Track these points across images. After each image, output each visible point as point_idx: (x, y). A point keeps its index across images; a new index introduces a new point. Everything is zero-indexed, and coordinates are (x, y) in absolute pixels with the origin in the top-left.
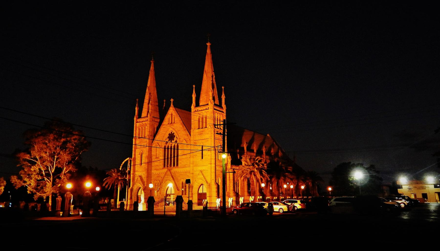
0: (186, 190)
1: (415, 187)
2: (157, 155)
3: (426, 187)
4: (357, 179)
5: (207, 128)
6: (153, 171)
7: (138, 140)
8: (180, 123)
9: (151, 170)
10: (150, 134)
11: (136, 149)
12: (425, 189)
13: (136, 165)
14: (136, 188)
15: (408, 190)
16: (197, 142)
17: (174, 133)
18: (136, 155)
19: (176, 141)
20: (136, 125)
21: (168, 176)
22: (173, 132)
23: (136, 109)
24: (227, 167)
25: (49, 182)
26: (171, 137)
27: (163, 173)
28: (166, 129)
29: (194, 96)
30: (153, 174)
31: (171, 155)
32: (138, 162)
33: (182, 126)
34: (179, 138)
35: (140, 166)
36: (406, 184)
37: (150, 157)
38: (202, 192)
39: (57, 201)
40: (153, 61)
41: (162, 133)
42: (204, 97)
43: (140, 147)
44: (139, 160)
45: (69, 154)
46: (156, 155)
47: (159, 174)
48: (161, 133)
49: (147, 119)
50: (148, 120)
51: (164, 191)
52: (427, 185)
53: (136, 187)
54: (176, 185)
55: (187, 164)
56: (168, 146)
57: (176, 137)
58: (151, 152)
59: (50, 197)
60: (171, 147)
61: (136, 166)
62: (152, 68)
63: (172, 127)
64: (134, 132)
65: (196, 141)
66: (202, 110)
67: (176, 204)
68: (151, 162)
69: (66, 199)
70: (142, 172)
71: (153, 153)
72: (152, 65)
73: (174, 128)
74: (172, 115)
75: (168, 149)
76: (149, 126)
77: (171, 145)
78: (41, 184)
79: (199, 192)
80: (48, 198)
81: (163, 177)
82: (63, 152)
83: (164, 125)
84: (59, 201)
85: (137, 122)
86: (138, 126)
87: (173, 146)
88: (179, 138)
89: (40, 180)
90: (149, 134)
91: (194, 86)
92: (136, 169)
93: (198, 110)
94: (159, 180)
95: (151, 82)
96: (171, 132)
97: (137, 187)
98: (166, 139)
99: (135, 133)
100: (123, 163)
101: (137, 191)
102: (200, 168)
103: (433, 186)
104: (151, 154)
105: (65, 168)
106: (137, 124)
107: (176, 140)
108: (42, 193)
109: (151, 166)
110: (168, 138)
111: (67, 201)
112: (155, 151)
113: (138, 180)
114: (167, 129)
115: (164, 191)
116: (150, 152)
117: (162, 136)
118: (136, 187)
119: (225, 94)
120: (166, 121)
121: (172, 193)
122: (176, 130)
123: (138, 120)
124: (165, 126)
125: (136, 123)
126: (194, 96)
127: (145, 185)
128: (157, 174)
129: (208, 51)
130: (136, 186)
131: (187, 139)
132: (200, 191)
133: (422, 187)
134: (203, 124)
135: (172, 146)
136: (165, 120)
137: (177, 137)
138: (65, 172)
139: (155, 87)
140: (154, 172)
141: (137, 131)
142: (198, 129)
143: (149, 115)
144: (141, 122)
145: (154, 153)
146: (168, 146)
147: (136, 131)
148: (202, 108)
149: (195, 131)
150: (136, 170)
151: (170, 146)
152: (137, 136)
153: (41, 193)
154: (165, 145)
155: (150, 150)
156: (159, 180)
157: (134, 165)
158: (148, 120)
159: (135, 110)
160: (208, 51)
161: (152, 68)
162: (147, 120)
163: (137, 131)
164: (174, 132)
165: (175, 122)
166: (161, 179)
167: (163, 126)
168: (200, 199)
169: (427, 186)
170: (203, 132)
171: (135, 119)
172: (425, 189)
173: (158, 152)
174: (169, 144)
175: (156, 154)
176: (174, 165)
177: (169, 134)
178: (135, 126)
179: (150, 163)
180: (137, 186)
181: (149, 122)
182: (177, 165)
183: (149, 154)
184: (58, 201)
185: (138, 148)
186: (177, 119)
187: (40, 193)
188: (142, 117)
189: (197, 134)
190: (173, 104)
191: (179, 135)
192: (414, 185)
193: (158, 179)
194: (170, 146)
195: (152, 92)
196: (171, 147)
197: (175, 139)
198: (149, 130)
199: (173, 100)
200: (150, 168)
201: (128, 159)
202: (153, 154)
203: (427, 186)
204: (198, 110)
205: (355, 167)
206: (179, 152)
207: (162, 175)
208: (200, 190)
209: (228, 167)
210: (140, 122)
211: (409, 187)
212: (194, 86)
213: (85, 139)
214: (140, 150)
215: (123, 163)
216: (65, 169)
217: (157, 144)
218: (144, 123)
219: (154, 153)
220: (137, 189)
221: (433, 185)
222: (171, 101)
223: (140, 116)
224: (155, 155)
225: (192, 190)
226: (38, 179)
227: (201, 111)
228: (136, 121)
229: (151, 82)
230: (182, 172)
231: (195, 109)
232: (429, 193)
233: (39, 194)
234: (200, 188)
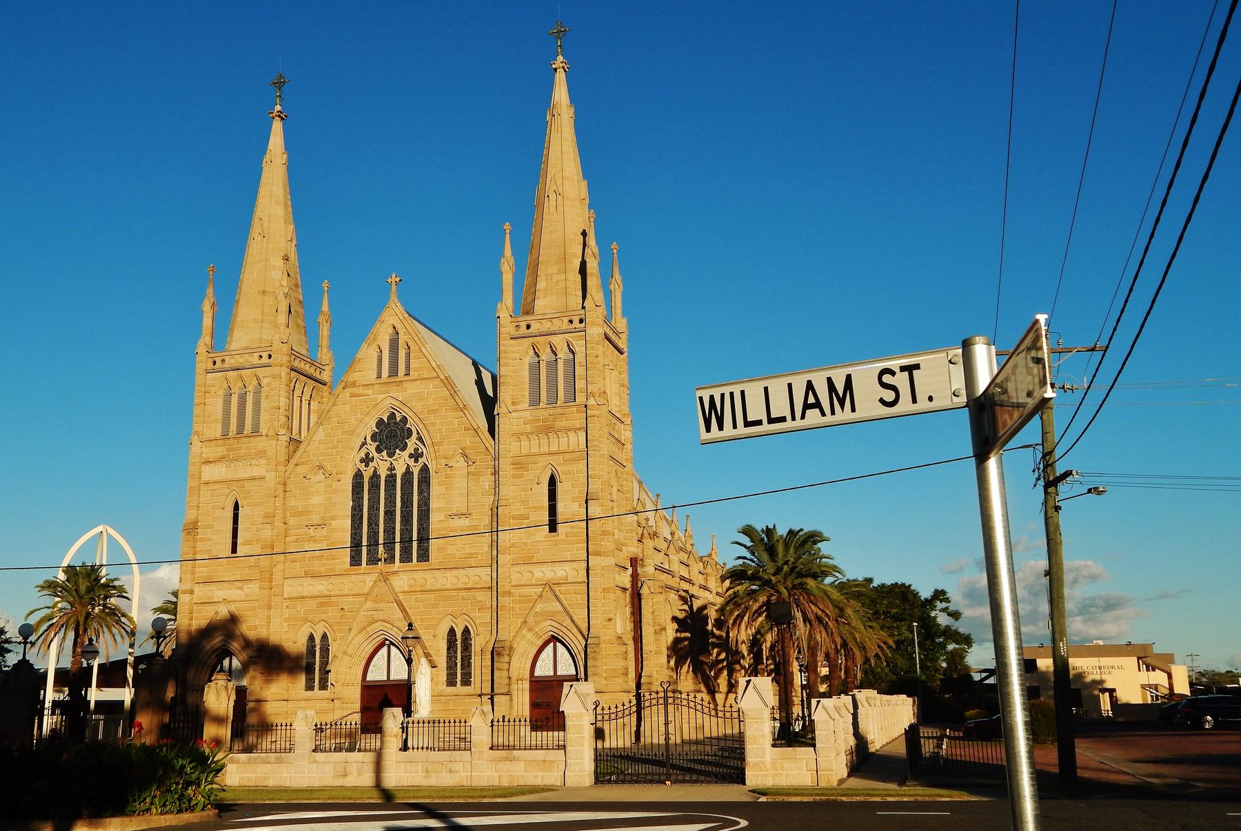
0: (469, 665)
17: (404, 420)
24: (639, 570)
38: (386, 679)
42: (555, 278)
54: (1052, 612)
56: (375, 476)
57: (415, 435)
60: (391, 478)
62: (561, 94)
72: (560, 77)
75: (375, 484)
77: (392, 469)
87: (400, 471)
96: (392, 416)
98: (364, 444)
107: (416, 450)
110: (374, 437)
137: (420, 439)
146: (375, 476)
151: (383, 473)
161: (561, 94)
174: (382, 465)
176: (406, 558)
177: (380, 423)
182: (424, 556)
194: (383, 473)
196: (391, 478)
197: (412, 443)
201: (100, 528)
205: (998, 596)
208: (538, 664)
209: (646, 569)
225: (509, 663)
234: (543, 656)
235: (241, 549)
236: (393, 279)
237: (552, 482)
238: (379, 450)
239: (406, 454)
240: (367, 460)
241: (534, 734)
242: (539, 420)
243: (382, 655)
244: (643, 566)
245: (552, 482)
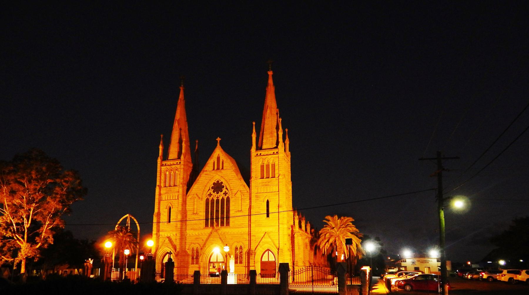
1: (419, 261)
2: (195, 209)
3: (429, 261)
4: (369, 251)
5: (275, 177)
6: (188, 231)
7: (163, 190)
8: (232, 170)
9: (186, 230)
10: (185, 182)
11: (161, 200)
12: (428, 263)
13: (160, 222)
14: (162, 253)
15: (411, 263)
16: (260, 195)
17: (222, 183)
18: (161, 209)
19: (225, 194)
20: (161, 171)
21: (215, 239)
22: (220, 180)
23: (161, 147)
24: (294, 230)
25: (20, 240)
26: (218, 187)
27: (202, 234)
28: (209, 177)
29: (254, 136)
30: (188, 235)
31: (217, 211)
32: (164, 217)
33: (235, 174)
34: (231, 190)
35: (167, 224)
36: (410, 257)
37: (184, 213)
38: (267, 260)
39: (86, 268)
40: (183, 88)
41: (204, 181)
43: (166, 199)
44: (165, 216)
45: (59, 201)
46: (194, 210)
47: (198, 236)
48: (201, 181)
49: (178, 162)
50: (180, 163)
51: (207, 258)
52: (431, 258)
53: (161, 252)
55: (244, 223)
57: (225, 187)
58: (186, 206)
59: (23, 263)
60: (218, 201)
61: (161, 224)
62: (181, 96)
63: (219, 174)
64: (158, 178)
65: (259, 194)
66: (267, 155)
67: (280, 274)
68: (186, 221)
69: (106, 265)
70: (171, 232)
71: (189, 207)
73: (222, 176)
74: (218, 158)
76: (182, 171)
77: (217, 198)
78: (7, 244)
79: (262, 260)
80: (19, 265)
81: (205, 239)
82: (52, 198)
83: (206, 171)
84: (89, 269)
85: (162, 165)
86: (163, 171)
87: (220, 198)
88: (231, 190)
89: (10, 238)
90: (183, 182)
91: (254, 123)
92: (161, 227)
93: (261, 154)
94: (198, 243)
95: (180, 114)
97: (164, 252)
99: (159, 179)
100: (121, 220)
101: (162, 258)
102: (264, 229)
103: (436, 260)
104: (186, 209)
105: (49, 222)
106: (162, 167)
107: (225, 192)
108: (9, 257)
109: (186, 224)
110: (212, 188)
111: (108, 269)
112: (192, 205)
113: (165, 242)
114: (211, 177)
115: (207, 257)
116: (184, 205)
117: (203, 186)
118: (161, 252)
119: (288, 138)
120: (209, 166)
121: (218, 261)
122: (226, 178)
123: (164, 163)
124: (208, 173)
125: (161, 166)
126: (254, 136)
127: (177, 250)
128: (195, 236)
129: (271, 81)
130: (162, 251)
131: (244, 192)
132: (265, 259)
133: (425, 261)
134: (165, 182)
135: (219, 200)
136: (208, 165)
137: (227, 188)
138: (46, 228)
139: (186, 121)
140: (189, 232)
141: (163, 178)
142: (261, 179)
143: (182, 157)
144: (168, 165)
145: (189, 208)
146: (213, 200)
147: (160, 177)
148: (268, 151)
149: (256, 180)
150: (160, 229)
152: (162, 185)
153: (8, 258)
154: (207, 197)
155: (184, 203)
156: (198, 243)
157: (158, 222)
158: (180, 163)
159: (251, 138)
160: (271, 81)
161: (181, 96)
162: (178, 163)
163: (163, 178)
164: (222, 180)
165: (224, 168)
166: (202, 241)
167: (205, 173)
168: (263, 268)
169: (430, 260)
170: (269, 182)
171: (159, 160)
172: (428, 263)
173: (195, 207)
174: (215, 196)
175: (194, 208)
177: (214, 184)
178: (159, 170)
179: (184, 221)
180: (164, 251)
181: (182, 167)
183: (182, 209)
184: (88, 267)
185: (164, 199)
186: (229, 164)
187: (6, 258)
188: (170, 158)
189: (261, 185)
190: (220, 145)
191: (231, 185)
192: (417, 259)
193: (197, 242)
194: (215, 199)
195: (183, 128)
197: (224, 190)
198: (183, 176)
199: (220, 139)
200: (184, 227)
201: (127, 215)
202: (189, 209)
203: (430, 260)
204: (166, 164)
206: (292, 204)
207: (205, 237)
210: (167, 165)
211: (412, 261)
212: (254, 123)
213: (80, 184)
214: (167, 202)
215: (121, 220)
216: (47, 223)
217: (195, 196)
218: (173, 166)
219: (189, 208)
220: (162, 254)
221: (436, 260)
222: (217, 141)
223: (165, 157)
224: (192, 209)
225: (254, 257)
226: (7, 235)
227: (267, 156)
228: (161, 163)
229: (180, 114)
230: (236, 233)
231: (257, 153)
232: (432, 267)
233: (6, 259)
235: (270, 215)
236: (219, 139)
237: (268, 202)
238: (214, 192)
239: (222, 193)
240: (210, 195)
241: (263, 278)
242: (263, 183)
243: (266, 255)
244: (295, 228)
245: (268, 202)
